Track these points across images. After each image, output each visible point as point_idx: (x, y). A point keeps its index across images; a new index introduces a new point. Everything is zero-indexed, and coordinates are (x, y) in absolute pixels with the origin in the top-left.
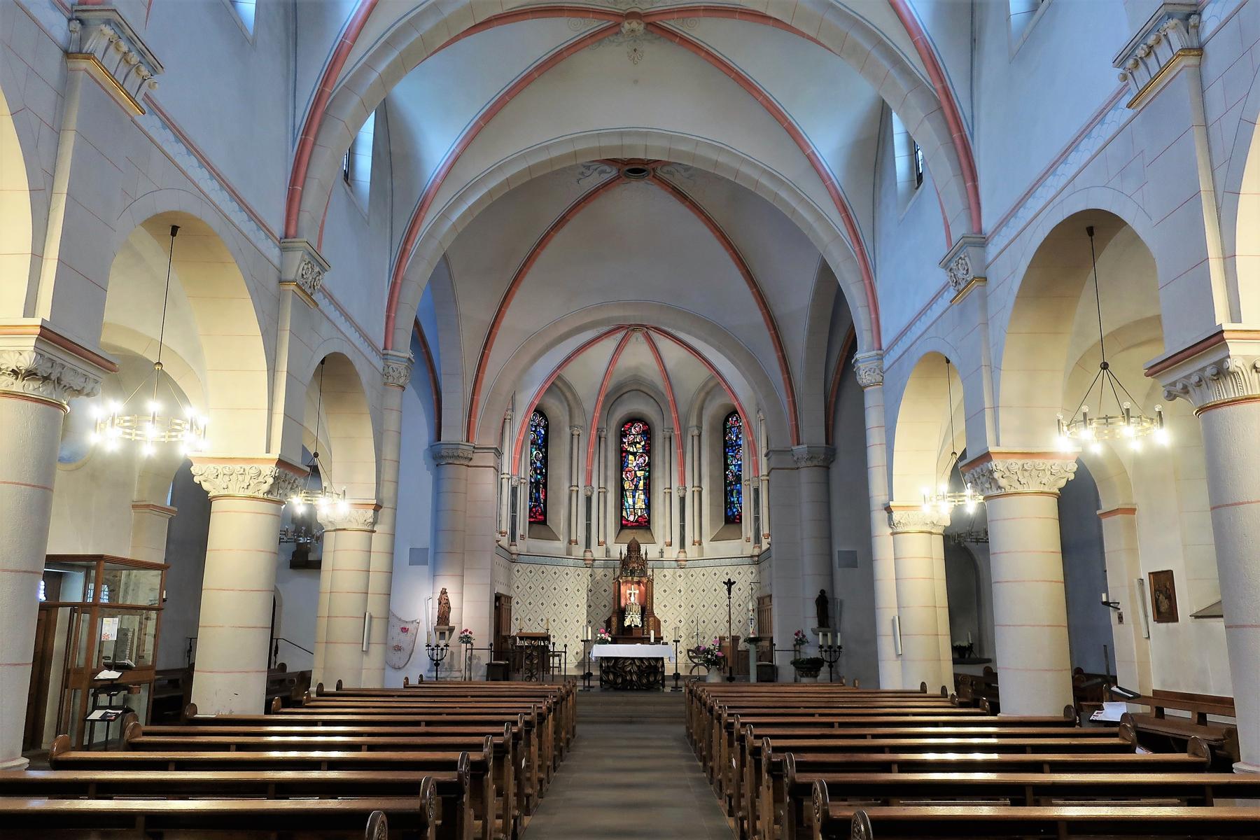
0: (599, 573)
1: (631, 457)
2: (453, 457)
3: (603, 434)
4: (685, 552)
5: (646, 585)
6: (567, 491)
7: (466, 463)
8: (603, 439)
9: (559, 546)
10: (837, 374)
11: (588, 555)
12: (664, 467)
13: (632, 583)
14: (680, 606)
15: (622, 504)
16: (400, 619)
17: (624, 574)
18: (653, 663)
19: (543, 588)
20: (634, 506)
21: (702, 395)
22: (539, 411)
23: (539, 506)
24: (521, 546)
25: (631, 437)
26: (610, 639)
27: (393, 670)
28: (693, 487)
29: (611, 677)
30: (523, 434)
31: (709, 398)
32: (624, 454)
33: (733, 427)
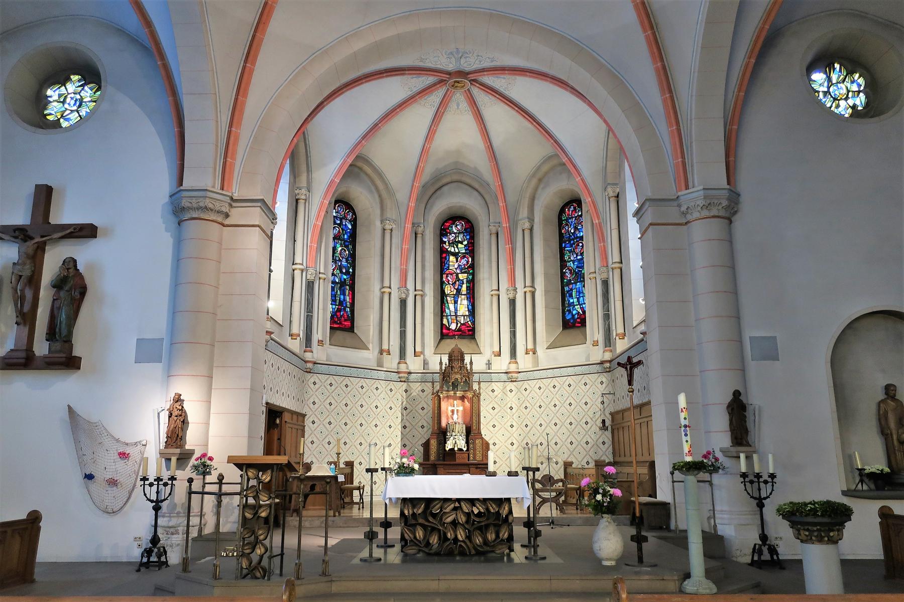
0: (416, 388)
1: (452, 258)
2: (199, 208)
3: (420, 230)
4: (516, 363)
5: (471, 401)
6: (377, 293)
7: (220, 219)
8: (419, 236)
9: (367, 357)
10: (739, 91)
11: (403, 367)
12: (490, 267)
13: (455, 398)
14: (512, 426)
15: (442, 311)
16: (118, 441)
17: (445, 388)
18: (493, 508)
19: (346, 405)
20: (456, 313)
21: (534, 181)
22: (343, 203)
23: (344, 310)
24: (318, 353)
25: (452, 237)
26: (416, 467)
27: (105, 515)
28: (525, 287)
29: (420, 533)
30: (321, 219)
31: (541, 186)
32: (444, 255)
33: (570, 218)
